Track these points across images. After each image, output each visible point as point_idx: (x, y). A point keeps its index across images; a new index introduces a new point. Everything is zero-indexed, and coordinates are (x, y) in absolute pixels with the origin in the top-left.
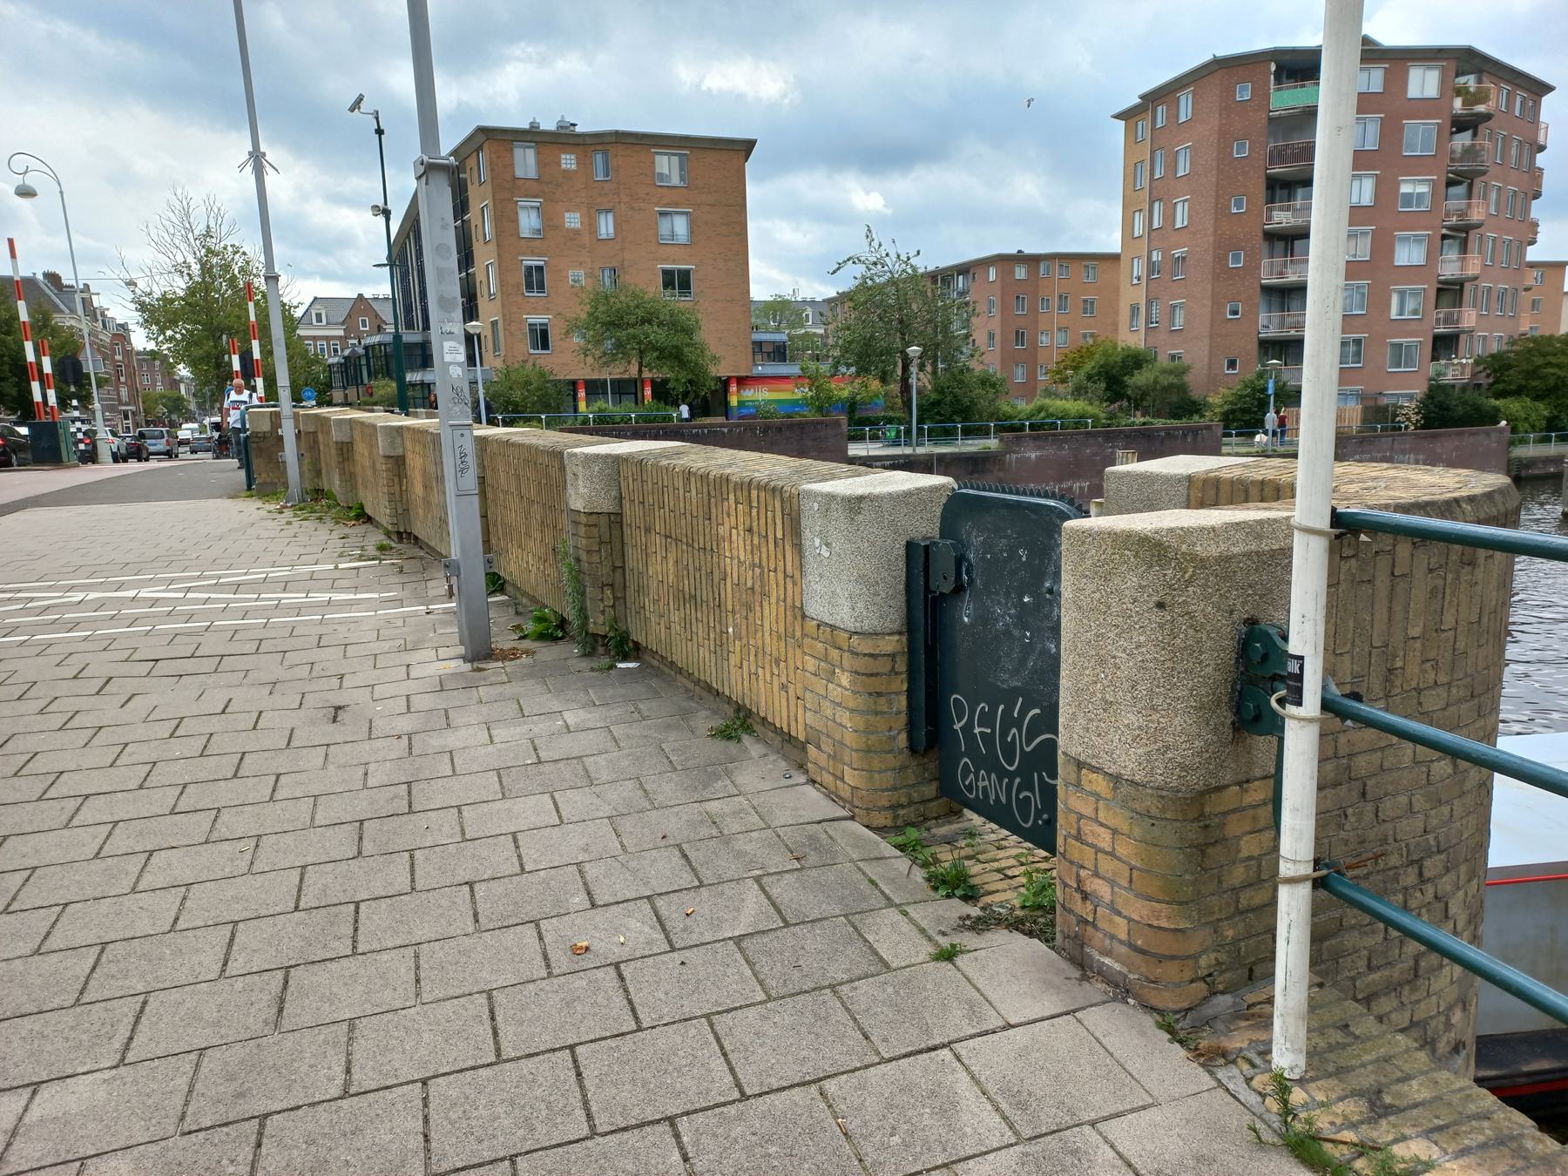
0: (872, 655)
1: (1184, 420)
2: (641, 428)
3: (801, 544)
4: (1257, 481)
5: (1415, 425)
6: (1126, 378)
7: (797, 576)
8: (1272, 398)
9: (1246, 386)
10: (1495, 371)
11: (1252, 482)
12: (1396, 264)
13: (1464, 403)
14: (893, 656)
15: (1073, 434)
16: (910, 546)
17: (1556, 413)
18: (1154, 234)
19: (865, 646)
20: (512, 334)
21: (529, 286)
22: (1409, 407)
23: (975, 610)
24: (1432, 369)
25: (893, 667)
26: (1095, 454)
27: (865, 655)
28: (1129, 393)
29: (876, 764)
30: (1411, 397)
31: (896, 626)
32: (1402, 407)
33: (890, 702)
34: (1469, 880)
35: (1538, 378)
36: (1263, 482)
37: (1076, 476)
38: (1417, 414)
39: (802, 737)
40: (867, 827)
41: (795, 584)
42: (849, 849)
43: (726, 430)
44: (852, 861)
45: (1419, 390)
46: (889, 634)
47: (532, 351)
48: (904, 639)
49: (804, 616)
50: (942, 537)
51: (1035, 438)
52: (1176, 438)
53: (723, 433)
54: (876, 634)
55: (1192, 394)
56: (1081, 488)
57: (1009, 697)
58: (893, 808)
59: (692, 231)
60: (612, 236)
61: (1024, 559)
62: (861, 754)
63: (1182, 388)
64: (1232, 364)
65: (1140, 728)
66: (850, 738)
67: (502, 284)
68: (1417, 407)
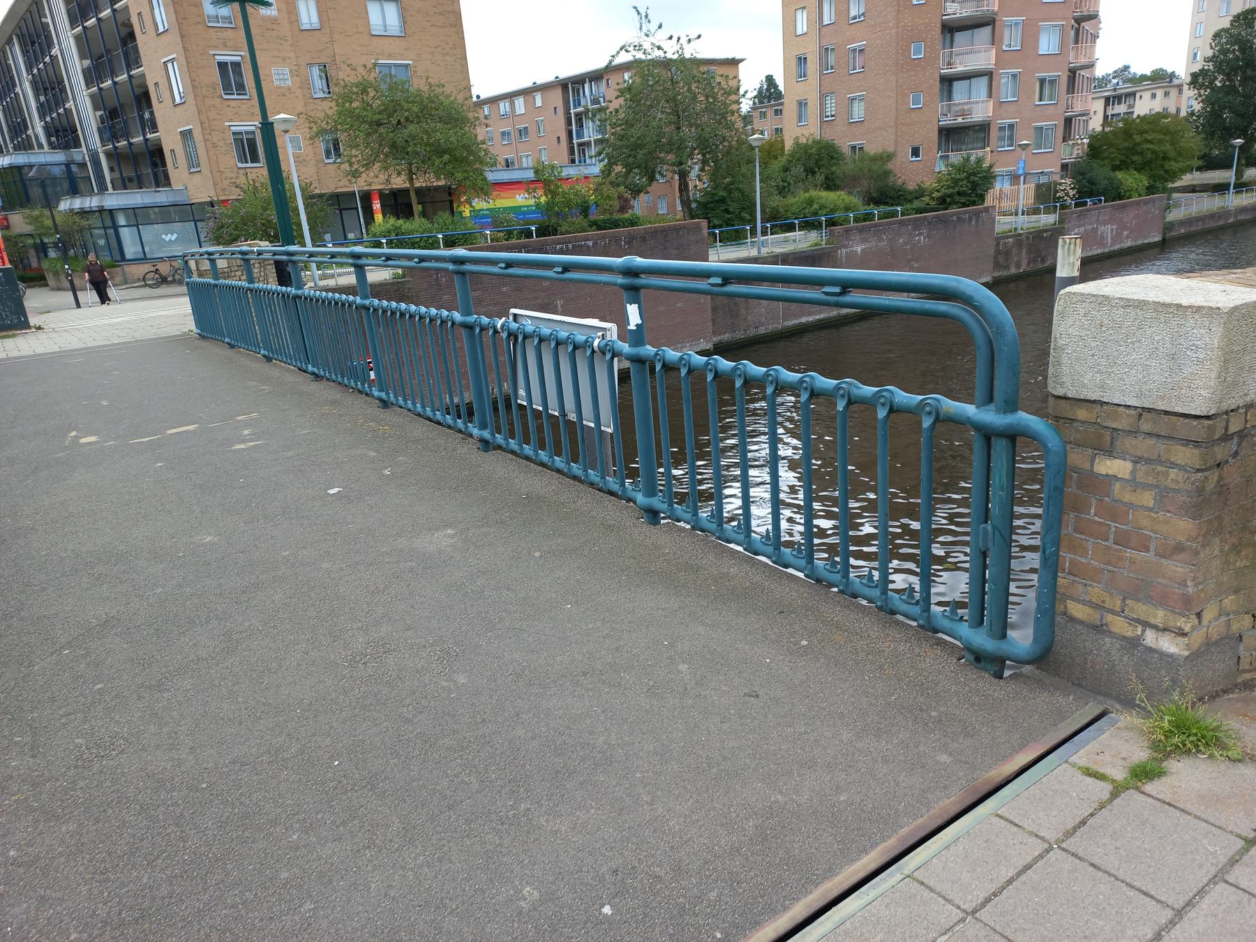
12: (1040, 53)
17: (1152, 183)
18: (825, 30)
20: (215, 146)
21: (227, 88)
24: (416, 217)
34: (406, 403)
35: (1137, 153)
38: (1073, 189)
43: (590, 243)
47: (240, 165)
51: (861, 230)
59: (404, 21)
60: (317, 26)
61: (164, 236)
64: (916, 152)
67: (194, 84)
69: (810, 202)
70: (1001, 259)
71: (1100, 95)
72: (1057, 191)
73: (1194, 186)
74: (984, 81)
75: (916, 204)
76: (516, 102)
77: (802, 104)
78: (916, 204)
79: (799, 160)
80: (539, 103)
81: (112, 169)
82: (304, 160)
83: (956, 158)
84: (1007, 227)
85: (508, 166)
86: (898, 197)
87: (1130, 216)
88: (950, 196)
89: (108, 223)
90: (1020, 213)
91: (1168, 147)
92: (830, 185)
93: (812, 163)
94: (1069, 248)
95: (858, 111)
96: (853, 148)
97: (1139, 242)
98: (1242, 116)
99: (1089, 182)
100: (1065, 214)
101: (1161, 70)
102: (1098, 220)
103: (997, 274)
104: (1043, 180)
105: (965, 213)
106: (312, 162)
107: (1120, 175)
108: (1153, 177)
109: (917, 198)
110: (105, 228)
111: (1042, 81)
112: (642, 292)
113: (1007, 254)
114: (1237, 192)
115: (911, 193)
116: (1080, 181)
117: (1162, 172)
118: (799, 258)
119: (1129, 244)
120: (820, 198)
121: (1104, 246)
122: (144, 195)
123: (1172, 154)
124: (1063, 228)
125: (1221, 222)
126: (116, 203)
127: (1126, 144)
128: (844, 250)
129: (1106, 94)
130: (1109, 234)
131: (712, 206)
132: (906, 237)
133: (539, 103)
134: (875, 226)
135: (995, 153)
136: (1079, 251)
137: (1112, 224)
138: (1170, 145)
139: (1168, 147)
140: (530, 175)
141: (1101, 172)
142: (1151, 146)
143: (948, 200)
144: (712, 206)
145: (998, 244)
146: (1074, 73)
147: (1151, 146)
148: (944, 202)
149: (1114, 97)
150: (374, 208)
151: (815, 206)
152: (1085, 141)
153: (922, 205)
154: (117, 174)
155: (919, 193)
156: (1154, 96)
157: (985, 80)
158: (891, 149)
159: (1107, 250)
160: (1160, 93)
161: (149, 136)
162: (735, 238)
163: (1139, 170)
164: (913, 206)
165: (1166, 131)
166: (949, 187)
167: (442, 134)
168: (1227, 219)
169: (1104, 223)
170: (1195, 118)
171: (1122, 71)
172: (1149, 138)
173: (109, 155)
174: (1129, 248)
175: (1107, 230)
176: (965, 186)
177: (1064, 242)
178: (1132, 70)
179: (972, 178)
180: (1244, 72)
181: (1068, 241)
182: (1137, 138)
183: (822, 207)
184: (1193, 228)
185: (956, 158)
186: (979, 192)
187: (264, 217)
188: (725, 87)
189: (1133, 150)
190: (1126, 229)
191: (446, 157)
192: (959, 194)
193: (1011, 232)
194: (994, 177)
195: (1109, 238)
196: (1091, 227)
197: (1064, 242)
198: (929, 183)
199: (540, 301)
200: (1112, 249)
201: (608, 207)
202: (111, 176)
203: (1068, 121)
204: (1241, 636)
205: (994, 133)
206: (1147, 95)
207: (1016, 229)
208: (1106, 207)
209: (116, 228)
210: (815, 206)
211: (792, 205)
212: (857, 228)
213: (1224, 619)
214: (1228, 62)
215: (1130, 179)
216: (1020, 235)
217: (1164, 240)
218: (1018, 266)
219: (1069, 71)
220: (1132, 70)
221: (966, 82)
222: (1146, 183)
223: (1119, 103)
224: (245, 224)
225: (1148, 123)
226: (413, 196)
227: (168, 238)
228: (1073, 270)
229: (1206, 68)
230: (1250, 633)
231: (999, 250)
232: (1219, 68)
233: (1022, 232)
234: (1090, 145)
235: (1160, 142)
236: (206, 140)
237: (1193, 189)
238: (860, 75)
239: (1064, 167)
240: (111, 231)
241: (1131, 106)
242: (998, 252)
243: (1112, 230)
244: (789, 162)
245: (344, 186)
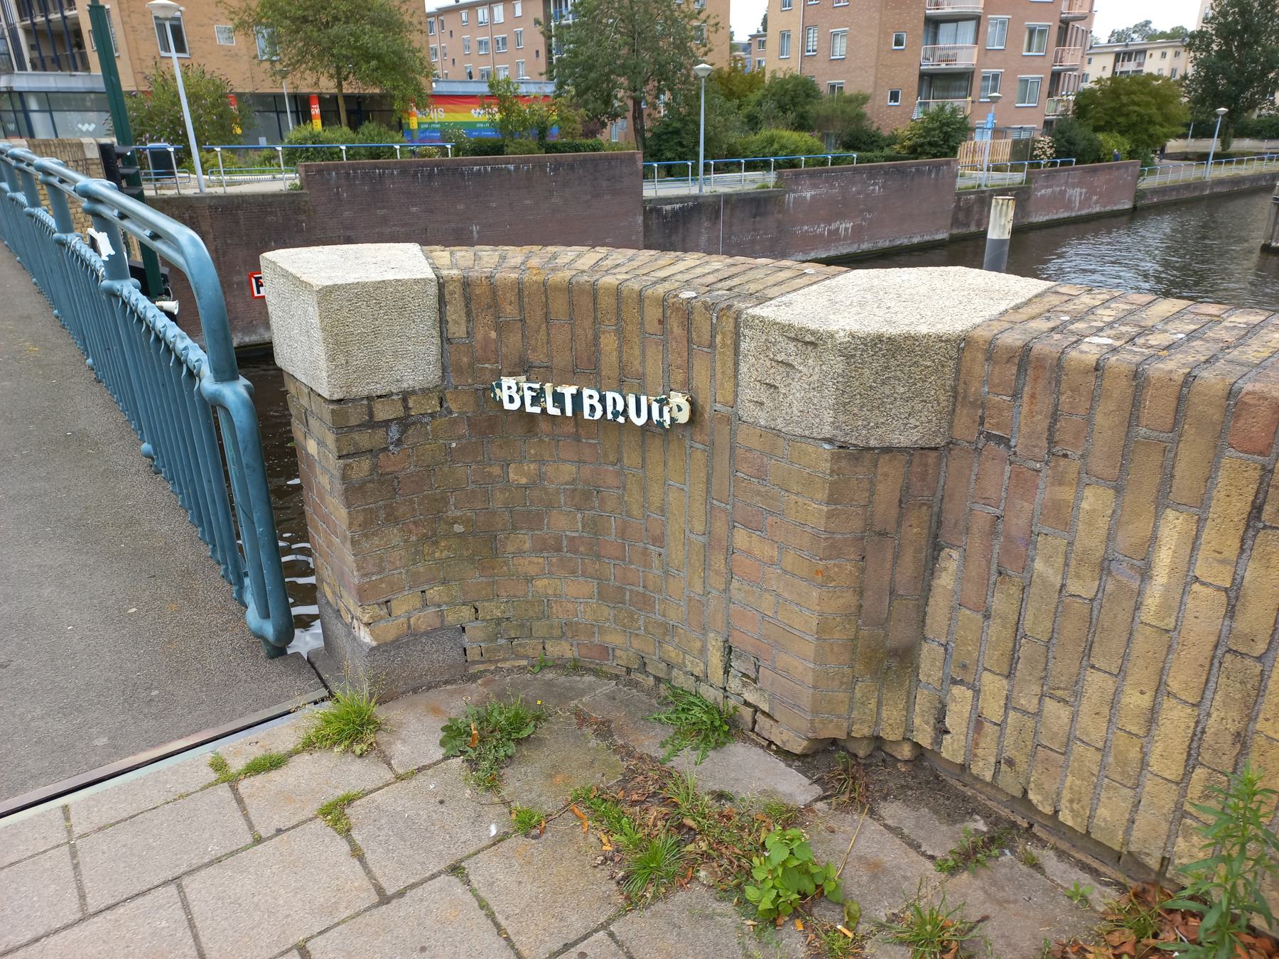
2: (410, 164)
17: (1134, 147)
20: (134, 30)
32: (1039, 142)
37: (841, 216)
38: (1051, 147)
43: (512, 167)
51: (812, 175)
53: (509, 171)
56: (846, 229)
61: (80, 126)
64: (894, 96)
69: (771, 141)
70: (961, 216)
71: (1109, 50)
72: (1034, 149)
73: (1187, 153)
74: (971, 25)
75: (887, 151)
76: (495, 10)
77: (785, 36)
78: (887, 151)
79: (774, 95)
80: (519, 12)
81: (32, 48)
82: (236, 55)
83: (933, 105)
84: (970, 183)
85: (471, 78)
86: (872, 143)
87: (1100, 181)
88: (922, 145)
89: (18, 106)
90: (985, 169)
91: (1154, 111)
92: (801, 125)
93: (787, 99)
94: (1001, 209)
95: (840, 48)
96: (833, 87)
97: (1108, 208)
98: (1235, 83)
99: (1067, 141)
100: (1033, 173)
101: (1182, 28)
102: (1066, 183)
103: (955, 231)
104: (1024, 136)
105: (376, 167)
106: (246, 58)
107: (1101, 136)
108: (1137, 142)
109: (888, 145)
110: (15, 112)
111: (1032, 32)
113: (968, 211)
114: (1215, 163)
115: (884, 140)
116: (1058, 140)
117: (1146, 137)
118: (744, 200)
119: (1097, 209)
120: (781, 137)
121: (1072, 210)
122: (57, 78)
123: (1159, 119)
124: (1029, 188)
125: (1196, 194)
126: (53, 85)
127: (1113, 105)
128: (792, 195)
129: (1117, 49)
130: (1078, 198)
131: (664, 137)
132: (859, 185)
133: (519, 12)
134: (827, 171)
135: (976, 104)
136: (1011, 213)
137: (1081, 188)
138: (1158, 109)
140: (484, 89)
141: (1082, 133)
142: (1136, 108)
143: (919, 149)
144: (664, 137)
145: (959, 199)
146: (1067, 24)
147: (1136, 108)
148: (915, 151)
149: (1125, 53)
150: (313, 113)
151: (776, 146)
152: (1070, 98)
153: (893, 153)
154: (36, 54)
155: (892, 140)
156: (1164, 55)
157: (972, 24)
158: (869, 91)
159: (1073, 214)
160: (1170, 52)
161: (67, 13)
162: (671, 172)
163: (1122, 133)
164: (884, 154)
165: (1155, 93)
166: (921, 136)
167: (372, 38)
168: (1202, 190)
170: (1187, 82)
171: (1143, 26)
172: (1136, 99)
173: (27, 31)
174: (1097, 213)
175: (1076, 193)
176: (936, 137)
177: (997, 203)
178: (1153, 26)
179: (945, 129)
180: (1242, 38)
181: (1001, 202)
182: (1124, 99)
183: (783, 147)
184: (1166, 198)
185: (933, 105)
186: (952, 144)
187: (172, 113)
188: (686, 10)
189: (1118, 111)
190: (1095, 193)
191: (374, 63)
192: (930, 144)
193: (974, 187)
194: (973, 130)
196: (1058, 189)
197: (997, 203)
198: (903, 129)
199: (453, 225)
200: (1079, 213)
201: (570, 130)
202: (31, 54)
203: (1056, 76)
204: (464, 629)
205: (977, 82)
206: (1157, 54)
207: (979, 186)
208: (1076, 170)
209: (26, 112)
210: (776, 146)
211: (752, 142)
212: (807, 172)
213: (432, 610)
214: (1226, 25)
215: (1112, 142)
216: (983, 192)
217: (1135, 208)
219: (1061, 21)
220: (1153, 26)
221: (953, 25)
222: (1128, 147)
223: (1129, 60)
224: (152, 119)
225: (1138, 83)
226: (341, 102)
227: (85, 127)
228: (1003, 233)
229: (1204, 29)
230: (474, 624)
232: (1219, 32)
233: (985, 189)
234: (1076, 103)
235: (1148, 104)
236: (124, 23)
237: (1184, 157)
238: (844, 9)
239: (1048, 124)
240: (21, 116)
241: (1140, 64)
242: (958, 208)
243: (1081, 194)
244: (764, 96)
245: (267, 87)
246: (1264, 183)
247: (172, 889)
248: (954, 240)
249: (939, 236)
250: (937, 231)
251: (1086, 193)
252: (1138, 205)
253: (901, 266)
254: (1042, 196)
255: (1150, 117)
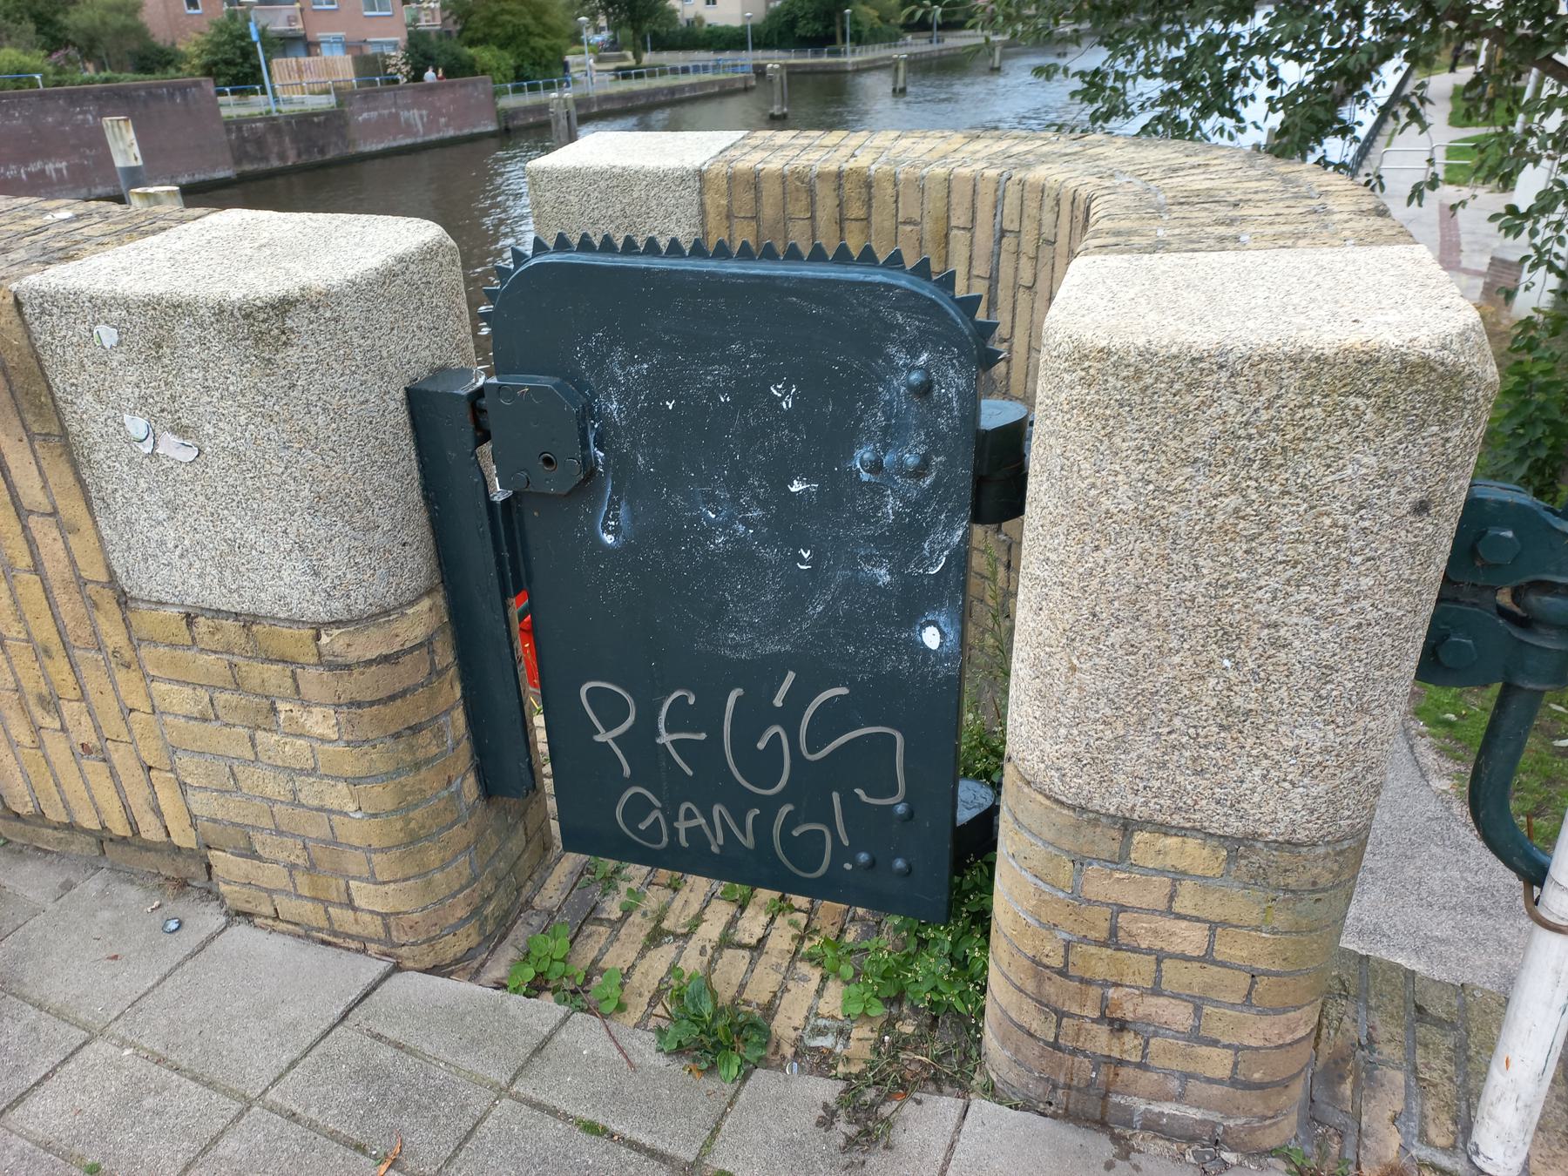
0: (385, 659)
1: (158, 75)
3: (64, 433)
4: (829, 173)
5: (406, 76)
6: (60, 17)
7: (72, 508)
8: (259, 46)
9: (221, 31)
10: (460, 17)
11: (819, 176)
13: (444, 52)
14: (427, 644)
15: (14, 96)
16: (416, 399)
17: (519, 62)
19: (369, 645)
22: (397, 56)
23: (634, 518)
25: (432, 662)
26: (62, 124)
27: (369, 663)
28: (71, 37)
29: (433, 856)
30: (395, 45)
31: (421, 582)
32: (390, 57)
33: (439, 734)
35: (498, 26)
36: (839, 175)
39: (184, 837)
40: (435, 970)
41: (66, 529)
42: (466, 1061)
44: (502, 1092)
45: (401, 38)
46: (411, 603)
48: (439, 599)
49: (124, 600)
50: (503, 358)
52: (160, 98)
54: (387, 612)
55: (154, 39)
57: (760, 675)
58: (476, 912)
62: (396, 853)
63: (140, 32)
65: (1325, 750)
66: (355, 829)
68: (404, 57)
72: (387, 67)
88: (215, 64)
91: (529, 20)
97: (466, 131)
102: (395, 104)
112: (1005, 227)
123: (534, 28)
137: (419, 109)
139: (529, 20)
143: (214, 69)
147: (508, 17)
159: (419, 140)
168: (588, 107)
169: (408, 108)
175: (415, 116)
176: (229, 52)
195: (420, 126)
196: (386, 112)
216: (274, 119)
218: (282, 156)
222: (512, 62)
231: (243, 137)
243: (421, 117)
246: (663, 98)
247: (1177, 908)
248: (242, 180)
249: (220, 174)
250: (214, 168)
251: (428, 116)
252: (510, 126)
253: (315, 210)
254: (364, 120)
255: (526, 26)
